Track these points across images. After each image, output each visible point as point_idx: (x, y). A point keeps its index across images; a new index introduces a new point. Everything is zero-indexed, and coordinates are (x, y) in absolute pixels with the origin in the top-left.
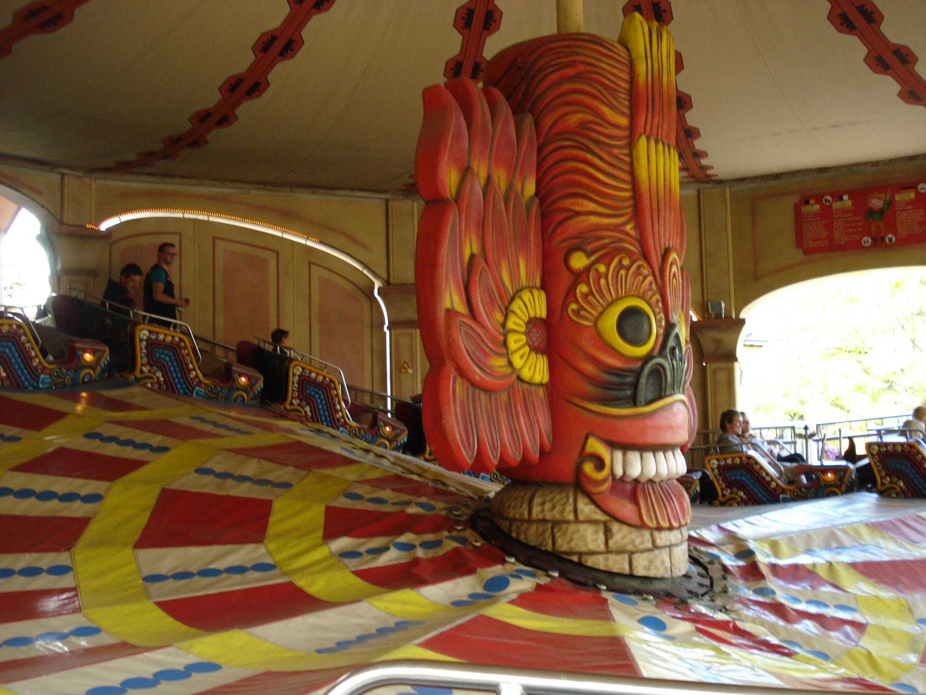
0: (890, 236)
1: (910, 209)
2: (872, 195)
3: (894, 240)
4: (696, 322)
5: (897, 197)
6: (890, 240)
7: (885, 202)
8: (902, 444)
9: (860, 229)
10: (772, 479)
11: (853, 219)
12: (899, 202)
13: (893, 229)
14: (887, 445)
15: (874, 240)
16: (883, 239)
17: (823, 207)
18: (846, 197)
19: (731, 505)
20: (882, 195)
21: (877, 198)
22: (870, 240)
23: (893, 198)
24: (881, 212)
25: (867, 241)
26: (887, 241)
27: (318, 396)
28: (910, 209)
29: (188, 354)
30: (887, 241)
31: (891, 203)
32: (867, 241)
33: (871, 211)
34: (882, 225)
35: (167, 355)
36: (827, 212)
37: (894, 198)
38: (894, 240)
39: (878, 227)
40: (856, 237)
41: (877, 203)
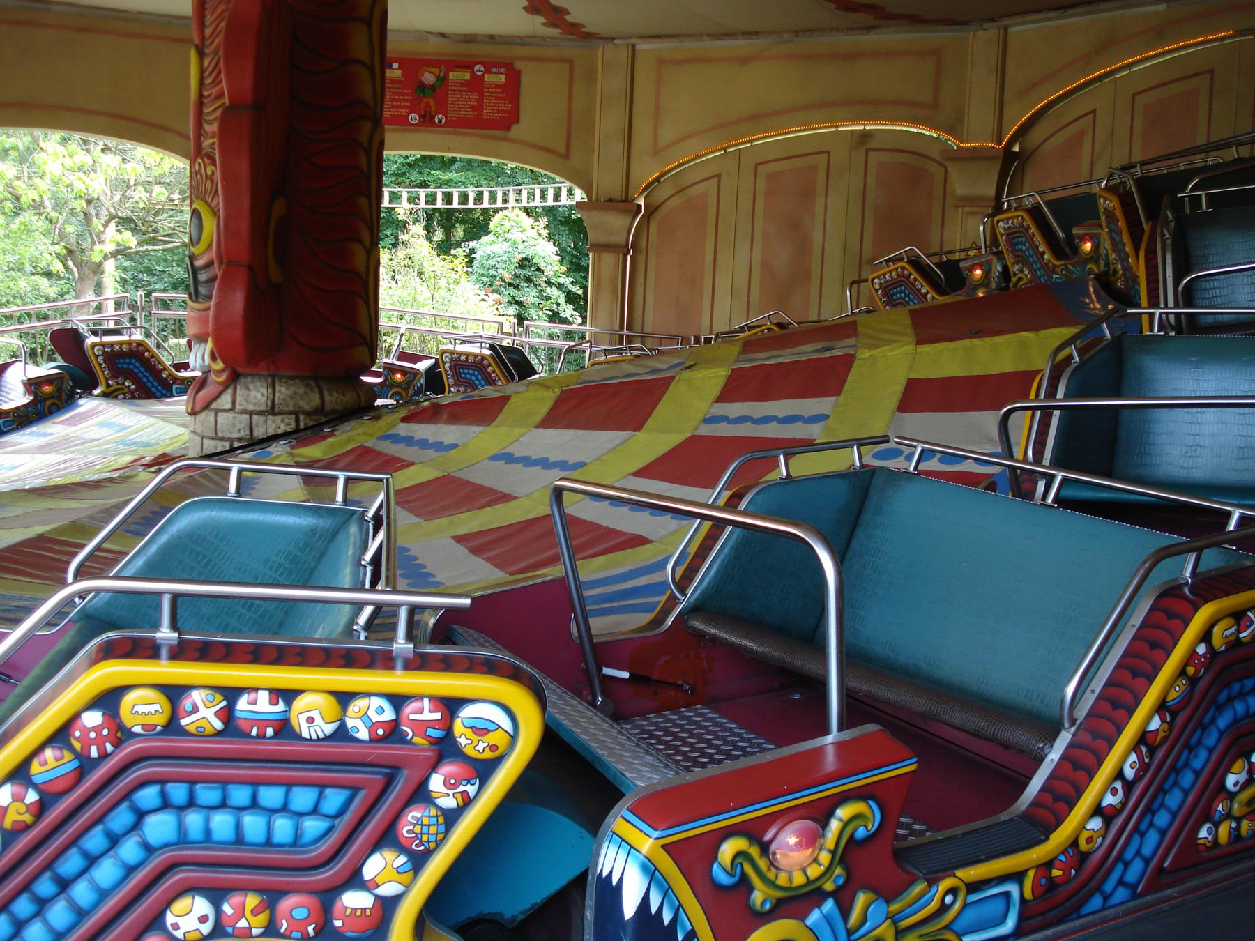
0: (440, 116)
1: (464, 91)
2: (425, 68)
3: (443, 121)
4: (959, 265)
5: (452, 76)
6: (440, 121)
7: (438, 78)
8: (476, 356)
9: (408, 104)
10: (164, 369)
11: (501, 95)
12: (453, 81)
13: (442, 108)
14: (460, 354)
15: (422, 117)
16: (433, 117)
17: (473, 75)
18: (395, 65)
19: (116, 397)
20: (436, 71)
21: (430, 72)
22: (418, 118)
23: (446, 76)
24: (432, 87)
25: (414, 118)
26: (437, 120)
27: (135, 365)
28: (464, 91)
29: (494, 372)
30: (437, 120)
31: (443, 80)
32: (414, 118)
33: (422, 86)
34: (432, 103)
35: (473, 375)
36: (476, 84)
37: (448, 76)
38: (443, 121)
39: (428, 104)
40: (403, 112)
41: (428, 78)
